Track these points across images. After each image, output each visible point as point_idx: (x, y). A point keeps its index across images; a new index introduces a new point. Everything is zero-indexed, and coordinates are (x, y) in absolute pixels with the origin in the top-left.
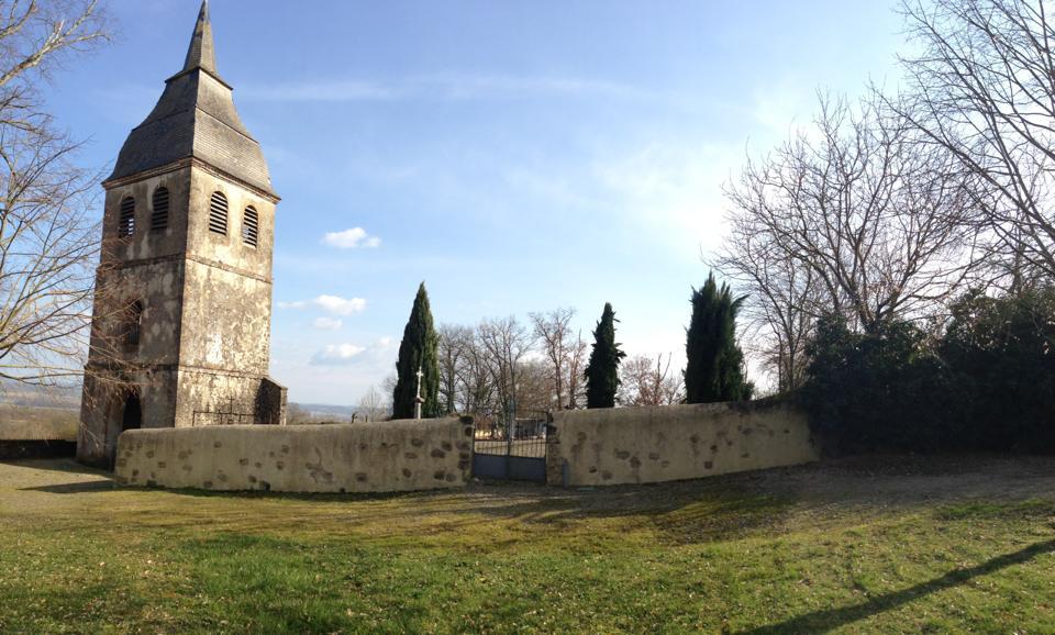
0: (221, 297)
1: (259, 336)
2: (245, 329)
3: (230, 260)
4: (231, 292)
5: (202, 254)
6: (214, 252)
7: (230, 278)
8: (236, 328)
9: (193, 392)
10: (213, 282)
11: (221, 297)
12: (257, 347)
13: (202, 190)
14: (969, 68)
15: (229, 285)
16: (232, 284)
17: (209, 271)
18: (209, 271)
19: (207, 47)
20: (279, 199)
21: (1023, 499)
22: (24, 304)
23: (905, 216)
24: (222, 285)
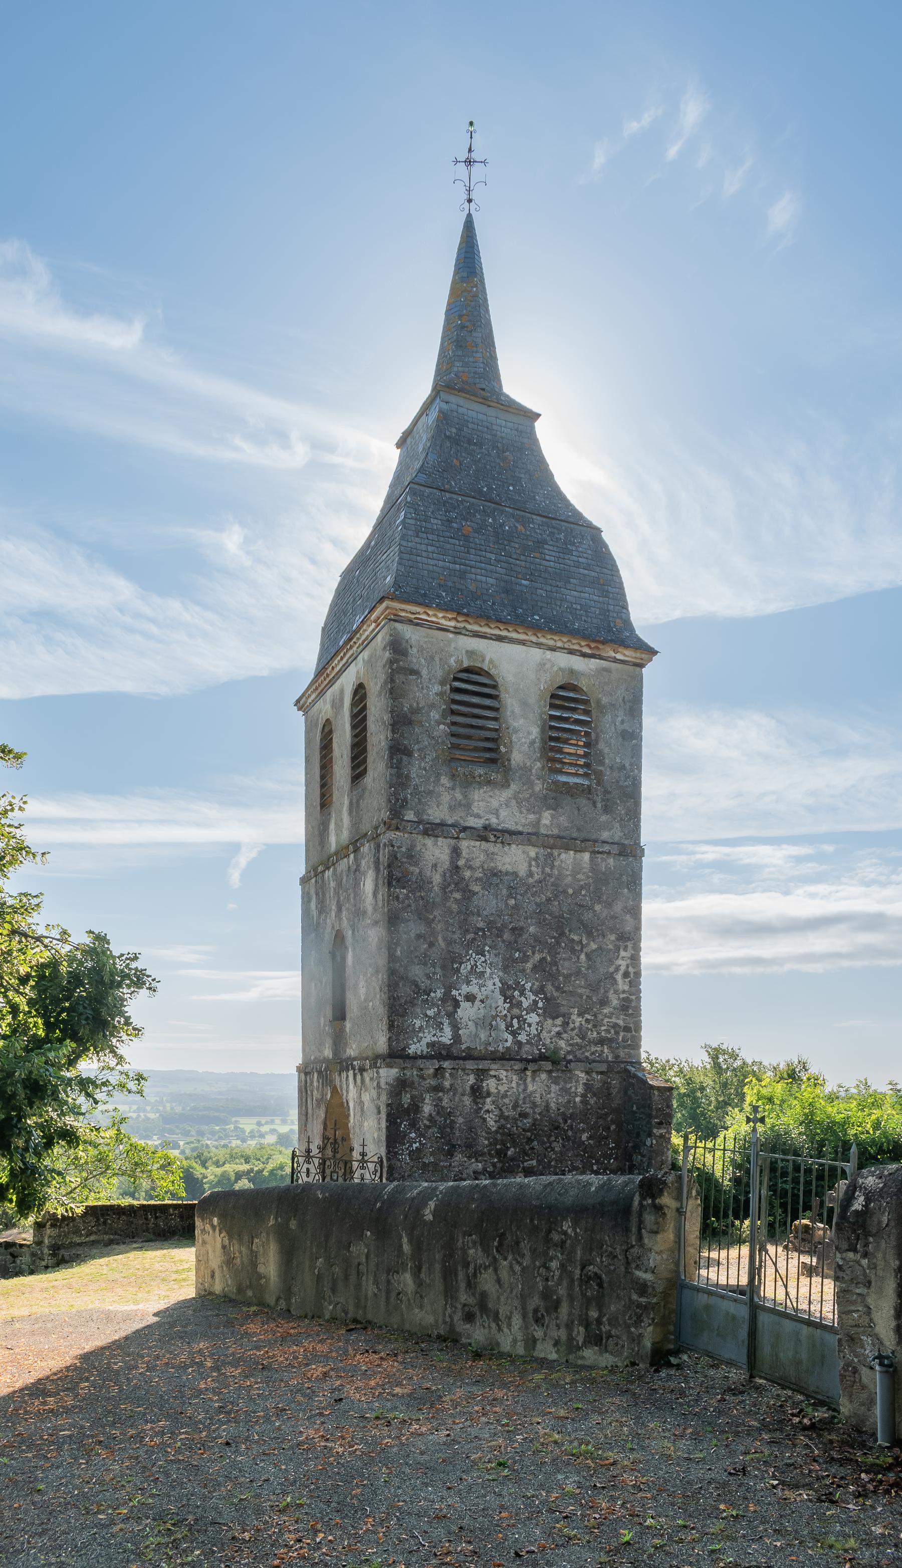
0: (489, 903)
1: (611, 977)
2: (565, 967)
3: (510, 818)
4: (514, 885)
5: (436, 813)
6: (468, 806)
7: (515, 859)
8: (539, 967)
9: (427, 1109)
10: (467, 874)
11: (489, 903)
12: (604, 1002)
13: (424, 672)
14: (691, 1459)
15: (515, 874)
16: (522, 873)
17: (456, 852)
18: (456, 852)
19: (544, 653)
20: (655, 653)
21: (572, 1281)
22: (320, 1025)
23: (140, 1295)
24: (493, 877)
